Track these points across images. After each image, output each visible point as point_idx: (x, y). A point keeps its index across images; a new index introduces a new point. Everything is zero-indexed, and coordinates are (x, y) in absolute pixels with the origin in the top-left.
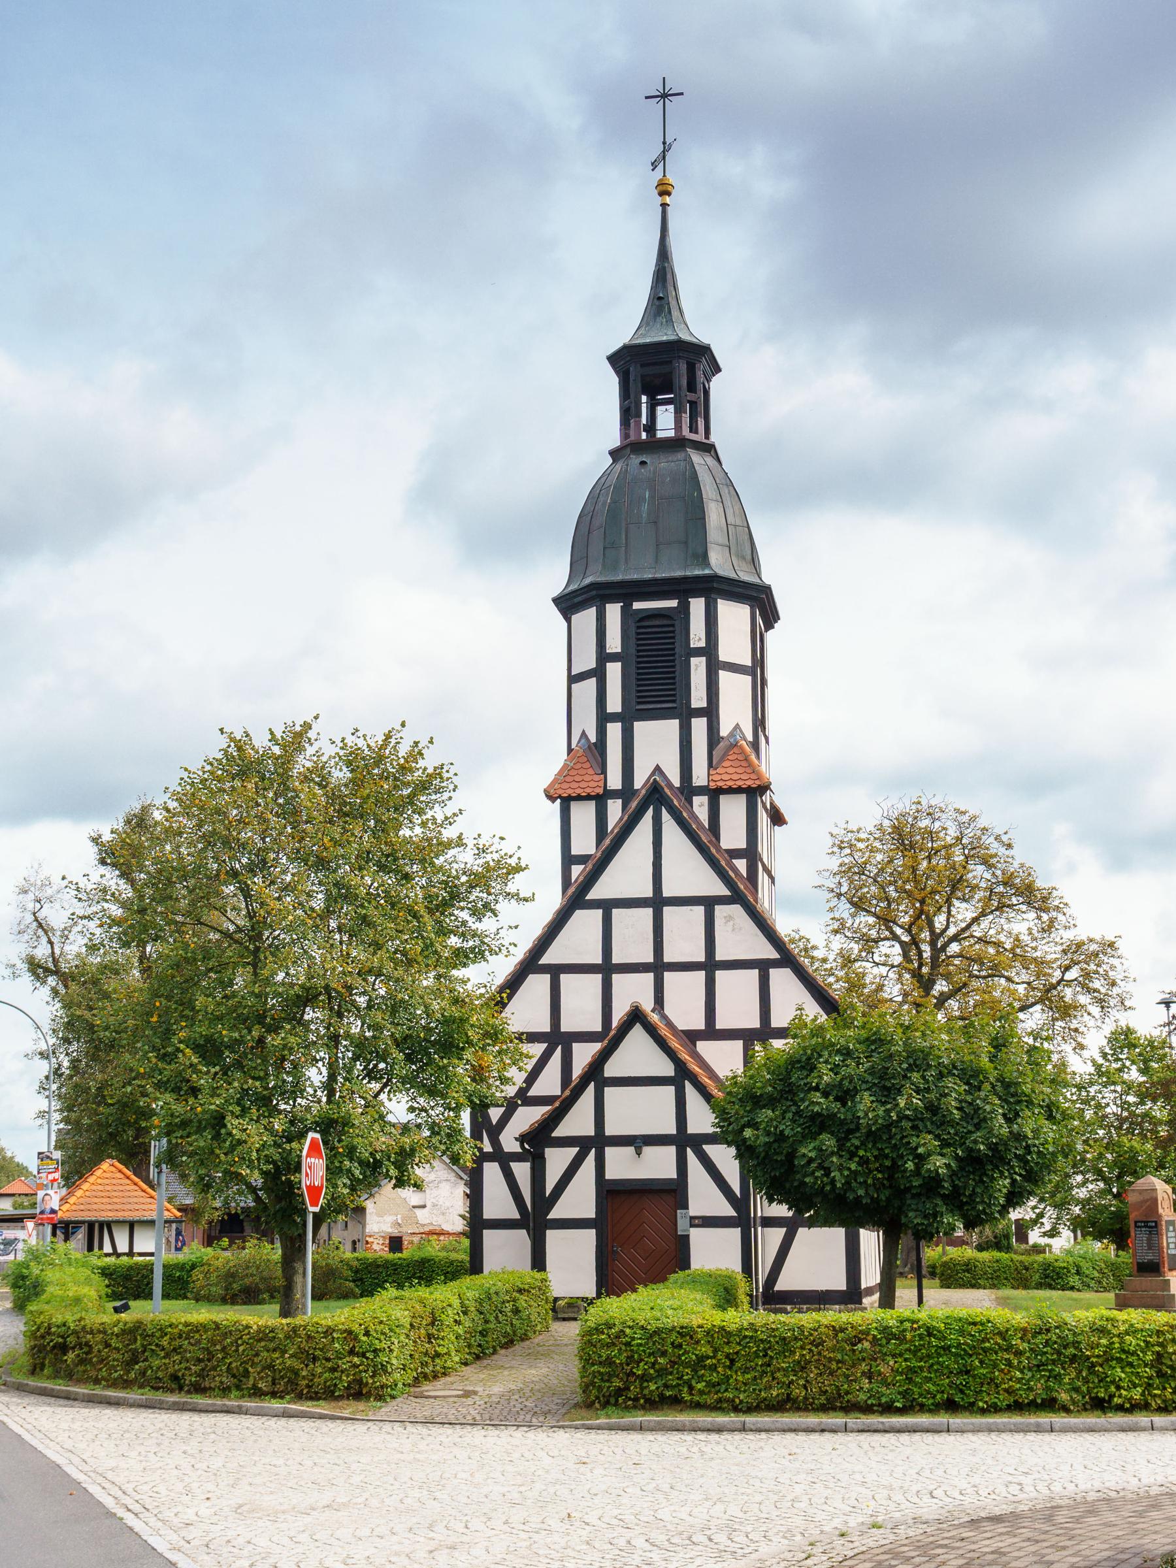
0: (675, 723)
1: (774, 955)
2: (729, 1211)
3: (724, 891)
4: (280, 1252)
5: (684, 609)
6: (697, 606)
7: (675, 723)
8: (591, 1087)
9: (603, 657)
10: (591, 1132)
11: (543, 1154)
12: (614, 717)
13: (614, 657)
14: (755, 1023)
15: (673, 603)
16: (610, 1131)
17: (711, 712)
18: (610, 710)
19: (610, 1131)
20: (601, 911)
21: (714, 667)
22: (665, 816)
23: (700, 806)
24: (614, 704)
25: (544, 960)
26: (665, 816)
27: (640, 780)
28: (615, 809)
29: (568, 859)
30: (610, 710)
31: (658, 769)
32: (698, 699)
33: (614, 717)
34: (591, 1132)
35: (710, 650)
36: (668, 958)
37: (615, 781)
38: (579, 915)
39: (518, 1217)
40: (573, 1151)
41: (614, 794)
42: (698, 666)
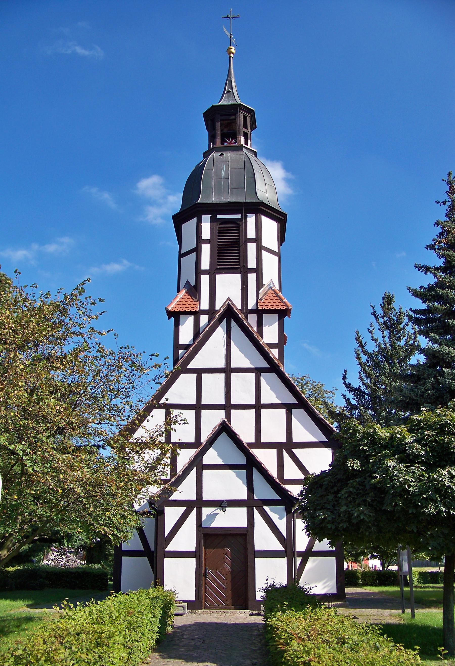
0: (238, 276)
1: (294, 401)
2: (279, 547)
3: (266, 365)
4: (355, 461)
5: (245, 218)
6: (251, 220)
7: (238, 276)
8: (195, 470)
9: (199, 241)
10: (193, 497)
11: (164, 510)
12: (205, 272)
13: (206, 242)
14: (283, 439)
15: (239, 216)
16: (206, 497)
17: (258, 271)
18: (254, 244)
19: (206, 497)
20: (195, 375)
21: (260, 249)
22: (233, 323)
23: (252, 320)
24: (205, 264)
25: (190, 366)
26: (233, 323)
27: (219, 305)
28: (204, 319)
29: (177, 346)
30: (254, 244)
31: (229, 299)
32: (252, 263)
33: (205, 272)
34: (193, 497)
35: (258, 240)
36: (234, 401)
37: (205, 305)
38: (183, 377)
39: (143, 549)
40: (182, 509)
41: (204, 312)
42: (252, 248)
